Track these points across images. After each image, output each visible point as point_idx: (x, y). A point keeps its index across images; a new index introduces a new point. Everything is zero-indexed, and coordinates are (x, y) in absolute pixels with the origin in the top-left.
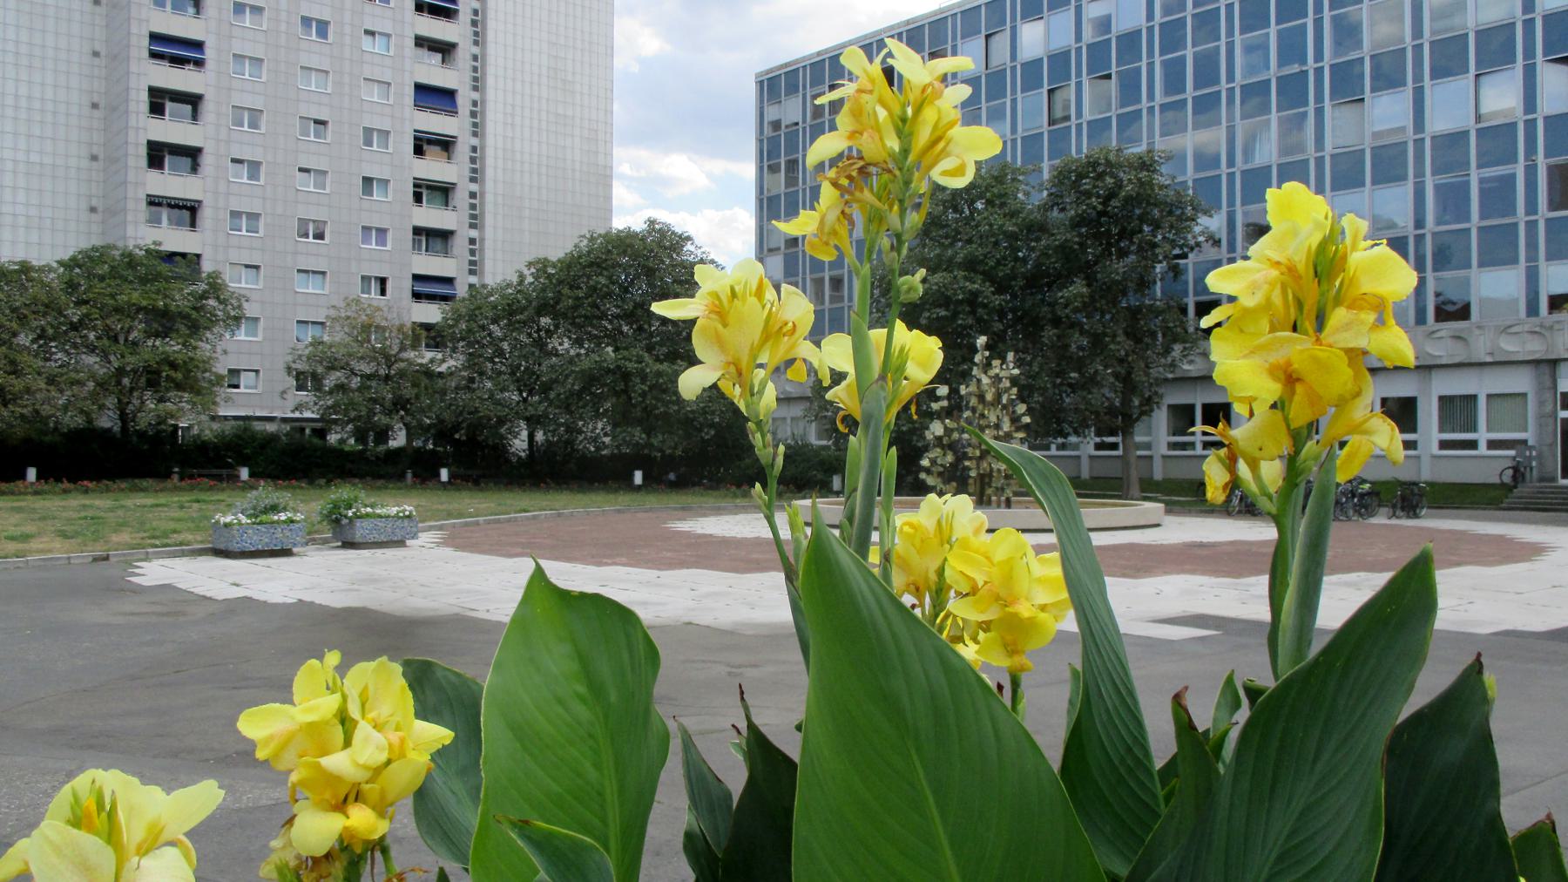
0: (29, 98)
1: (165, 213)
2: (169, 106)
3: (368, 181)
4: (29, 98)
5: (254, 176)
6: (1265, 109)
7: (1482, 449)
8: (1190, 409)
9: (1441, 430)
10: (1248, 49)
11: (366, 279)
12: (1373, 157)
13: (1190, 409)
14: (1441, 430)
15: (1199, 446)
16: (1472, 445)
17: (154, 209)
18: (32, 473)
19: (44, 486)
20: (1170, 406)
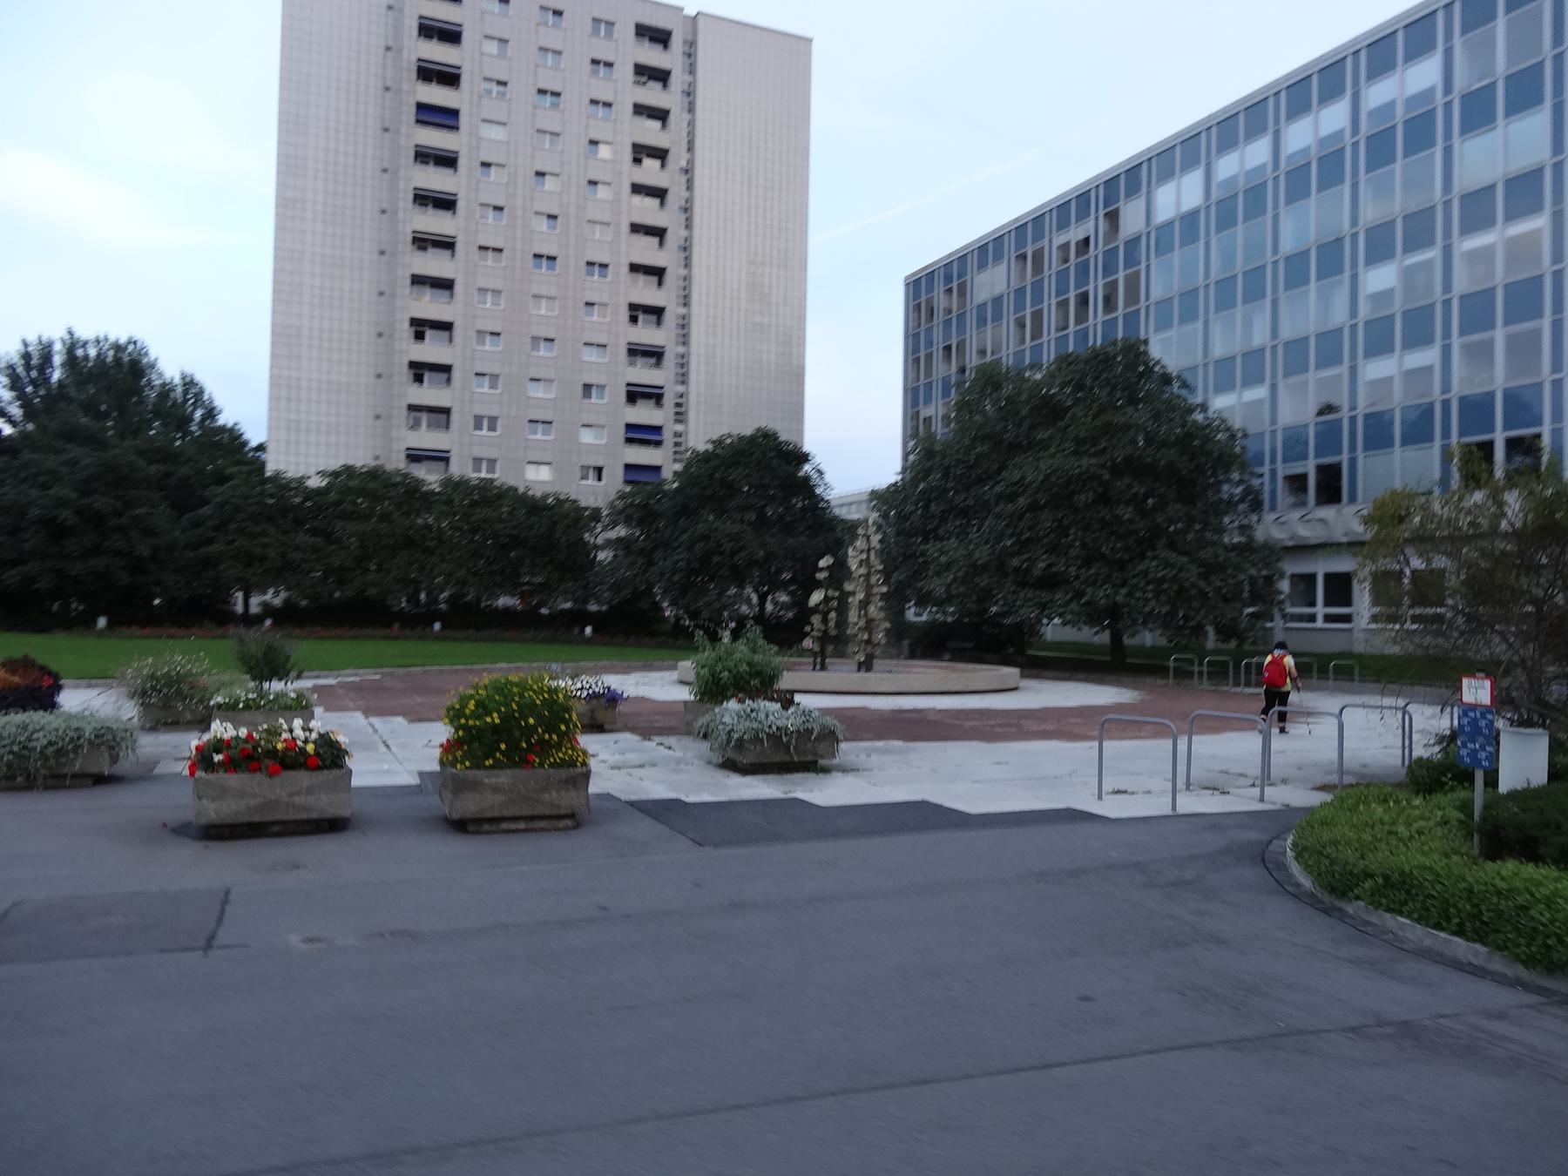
0: (331, 331)
1: (424, 417)
2: (429, 333)
3: (587, 388)
4: (331, 331)
5: (493, 386)
6: (1510, 396)
7: (1320, 623)
8: (1310, 579)
9: (1328, 577)
10: (1468, 350)
11: (585, 468)
12: (1367, 238)
13: (1310, 579)
14: (1328, 577)
15: (1320, 618)
16: (1312, 618)
17: (414, 414)
18: (102, 622)
19: (448, 633)
20: (1293, 576)
